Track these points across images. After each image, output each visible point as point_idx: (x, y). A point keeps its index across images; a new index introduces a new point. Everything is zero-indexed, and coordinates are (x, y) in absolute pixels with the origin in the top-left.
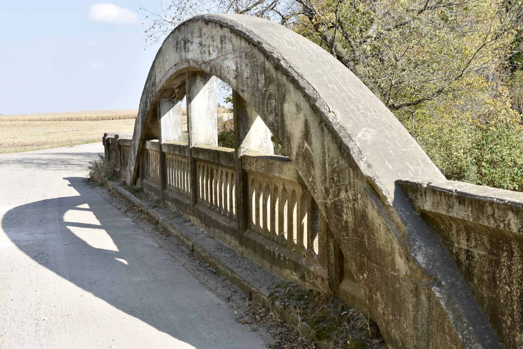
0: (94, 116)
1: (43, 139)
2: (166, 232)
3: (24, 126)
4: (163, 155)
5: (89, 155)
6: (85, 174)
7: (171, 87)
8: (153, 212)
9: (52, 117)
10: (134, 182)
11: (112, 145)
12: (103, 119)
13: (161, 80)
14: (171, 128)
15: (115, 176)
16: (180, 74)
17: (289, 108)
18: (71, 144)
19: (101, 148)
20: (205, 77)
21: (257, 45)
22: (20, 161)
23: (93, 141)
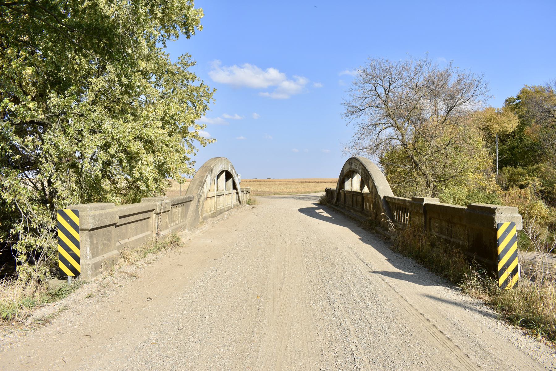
0: (317, 181)
1: (295, 190)
2: (345, 215)
3: (286, 184)
4: (345, 194)
5: (318, 197)
6: (318, 202)
7: (346, 175)
8: (341, 210)
9: (298, 181)
10: (336, 203)
11: (328, 191)
12: (321, 182)
13: (345, 172)
14: (348, 186)
15: (329, 202)
16: (350, 171)
17: (370, 182)
18: (309, 193)
19: (324, 193)
20: (357, 173)
21: (365, 168)
22: (293, 198)
23: (321, 192)
